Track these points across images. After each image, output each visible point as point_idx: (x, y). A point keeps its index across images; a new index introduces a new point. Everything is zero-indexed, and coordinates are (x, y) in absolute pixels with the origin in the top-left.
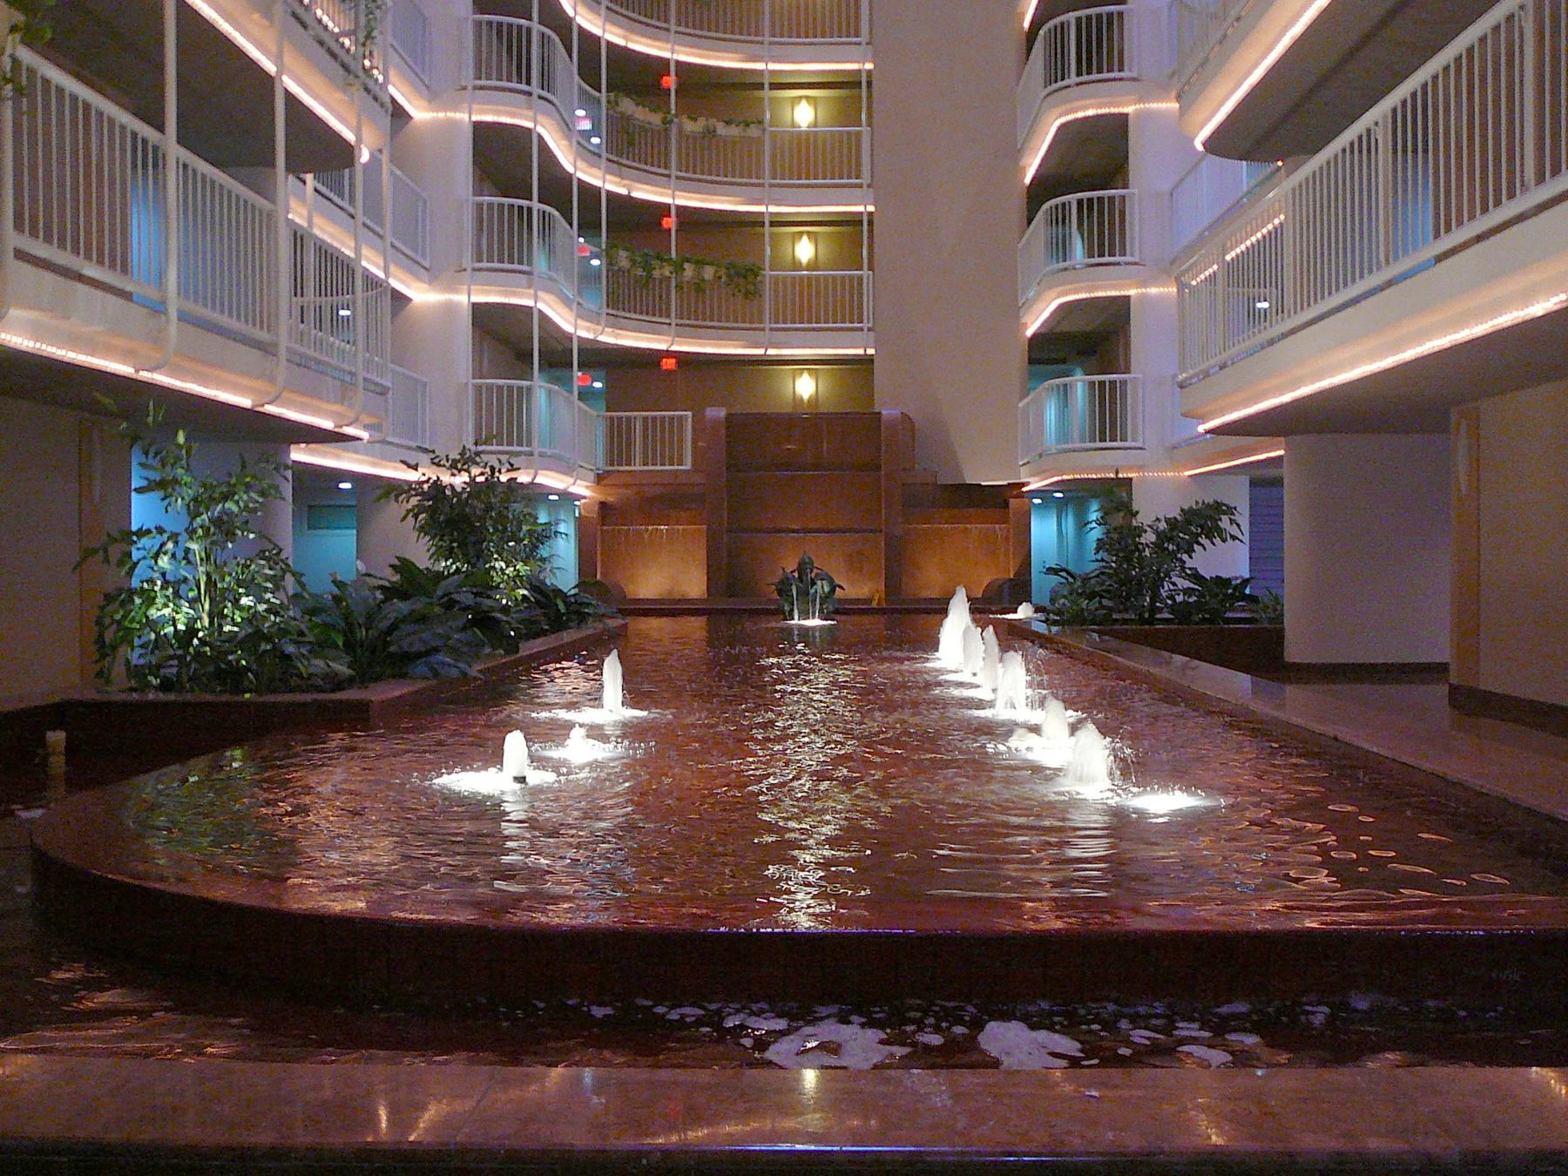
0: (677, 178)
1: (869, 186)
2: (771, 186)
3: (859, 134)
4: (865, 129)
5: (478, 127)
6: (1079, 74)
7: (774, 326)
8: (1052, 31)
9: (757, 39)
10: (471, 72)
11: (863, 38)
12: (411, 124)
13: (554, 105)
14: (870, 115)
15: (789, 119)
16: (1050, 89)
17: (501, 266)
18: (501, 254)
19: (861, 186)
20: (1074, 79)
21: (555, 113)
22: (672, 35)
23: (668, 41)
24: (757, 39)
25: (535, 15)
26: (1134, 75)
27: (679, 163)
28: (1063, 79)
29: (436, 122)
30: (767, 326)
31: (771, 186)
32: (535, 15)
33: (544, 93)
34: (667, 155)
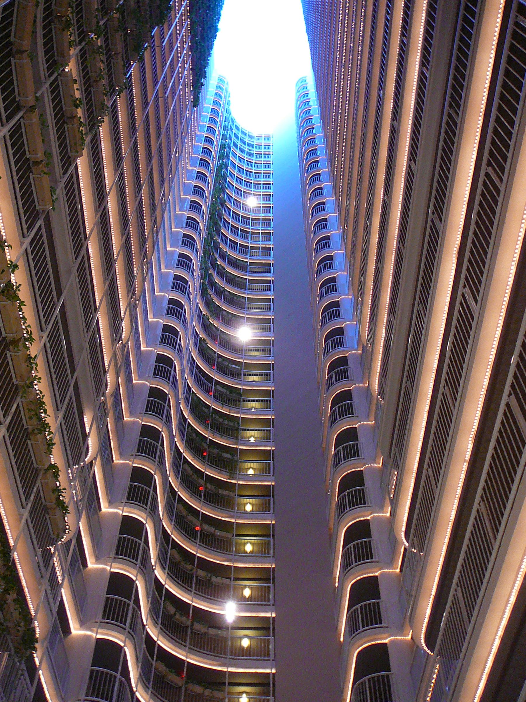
0: (194, 593)
1: (273, 605)
2: (235, 555)
3: (269, 541)
4: (272, 462)
5: (113, 575)
6: (356, 562)
7: (231, 657)
8: (361, 686)
9: (224, 656)
10: (84, 693)
11: (271, 511)
12: (87, 569)
13: (134, 639)
14: (273, 458)
15: (243, 550)
16: (352, 637)
17: (116, 623)
18: (117, 619)
19: (269, 605)
20: (361, 629)
21: (133, 641)
22: (187, 648)
23: (185, 650)
24: (224, 656)
25: (119, 672)
26: (377, 560)
27: (196, 587)
28: (357, 631)
29: (139, 384)
30: (228, 656)
31: (235, 555)
32: (119, 672)
33: (131, 631)
34: (186, 637)
